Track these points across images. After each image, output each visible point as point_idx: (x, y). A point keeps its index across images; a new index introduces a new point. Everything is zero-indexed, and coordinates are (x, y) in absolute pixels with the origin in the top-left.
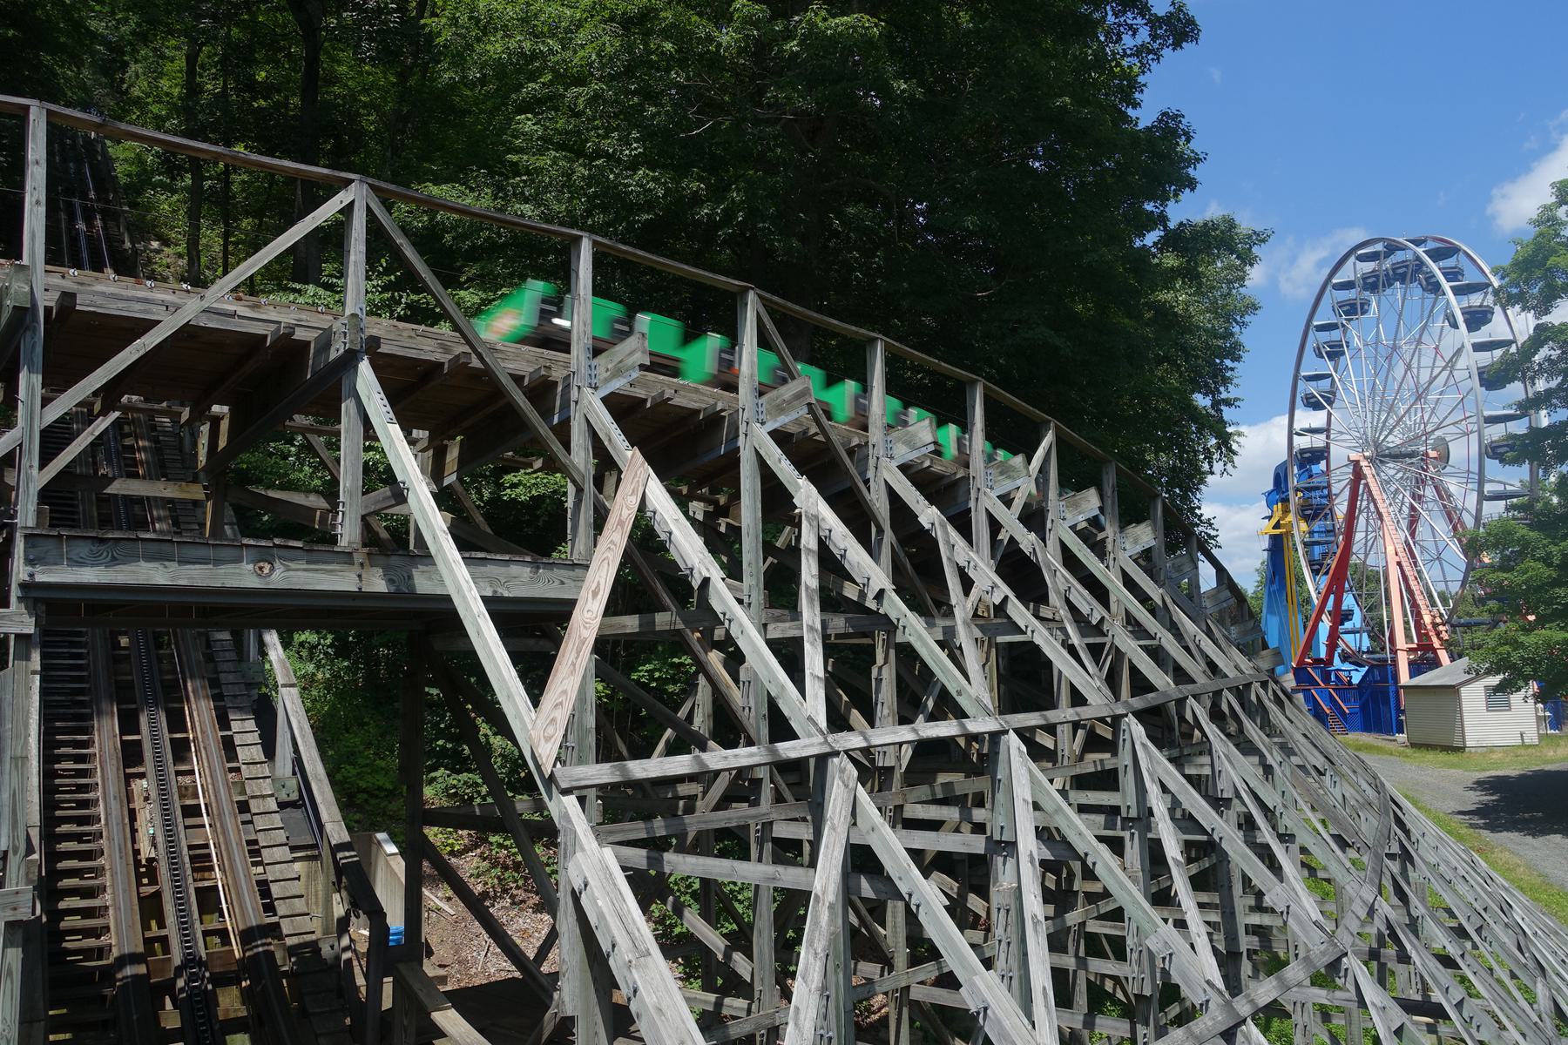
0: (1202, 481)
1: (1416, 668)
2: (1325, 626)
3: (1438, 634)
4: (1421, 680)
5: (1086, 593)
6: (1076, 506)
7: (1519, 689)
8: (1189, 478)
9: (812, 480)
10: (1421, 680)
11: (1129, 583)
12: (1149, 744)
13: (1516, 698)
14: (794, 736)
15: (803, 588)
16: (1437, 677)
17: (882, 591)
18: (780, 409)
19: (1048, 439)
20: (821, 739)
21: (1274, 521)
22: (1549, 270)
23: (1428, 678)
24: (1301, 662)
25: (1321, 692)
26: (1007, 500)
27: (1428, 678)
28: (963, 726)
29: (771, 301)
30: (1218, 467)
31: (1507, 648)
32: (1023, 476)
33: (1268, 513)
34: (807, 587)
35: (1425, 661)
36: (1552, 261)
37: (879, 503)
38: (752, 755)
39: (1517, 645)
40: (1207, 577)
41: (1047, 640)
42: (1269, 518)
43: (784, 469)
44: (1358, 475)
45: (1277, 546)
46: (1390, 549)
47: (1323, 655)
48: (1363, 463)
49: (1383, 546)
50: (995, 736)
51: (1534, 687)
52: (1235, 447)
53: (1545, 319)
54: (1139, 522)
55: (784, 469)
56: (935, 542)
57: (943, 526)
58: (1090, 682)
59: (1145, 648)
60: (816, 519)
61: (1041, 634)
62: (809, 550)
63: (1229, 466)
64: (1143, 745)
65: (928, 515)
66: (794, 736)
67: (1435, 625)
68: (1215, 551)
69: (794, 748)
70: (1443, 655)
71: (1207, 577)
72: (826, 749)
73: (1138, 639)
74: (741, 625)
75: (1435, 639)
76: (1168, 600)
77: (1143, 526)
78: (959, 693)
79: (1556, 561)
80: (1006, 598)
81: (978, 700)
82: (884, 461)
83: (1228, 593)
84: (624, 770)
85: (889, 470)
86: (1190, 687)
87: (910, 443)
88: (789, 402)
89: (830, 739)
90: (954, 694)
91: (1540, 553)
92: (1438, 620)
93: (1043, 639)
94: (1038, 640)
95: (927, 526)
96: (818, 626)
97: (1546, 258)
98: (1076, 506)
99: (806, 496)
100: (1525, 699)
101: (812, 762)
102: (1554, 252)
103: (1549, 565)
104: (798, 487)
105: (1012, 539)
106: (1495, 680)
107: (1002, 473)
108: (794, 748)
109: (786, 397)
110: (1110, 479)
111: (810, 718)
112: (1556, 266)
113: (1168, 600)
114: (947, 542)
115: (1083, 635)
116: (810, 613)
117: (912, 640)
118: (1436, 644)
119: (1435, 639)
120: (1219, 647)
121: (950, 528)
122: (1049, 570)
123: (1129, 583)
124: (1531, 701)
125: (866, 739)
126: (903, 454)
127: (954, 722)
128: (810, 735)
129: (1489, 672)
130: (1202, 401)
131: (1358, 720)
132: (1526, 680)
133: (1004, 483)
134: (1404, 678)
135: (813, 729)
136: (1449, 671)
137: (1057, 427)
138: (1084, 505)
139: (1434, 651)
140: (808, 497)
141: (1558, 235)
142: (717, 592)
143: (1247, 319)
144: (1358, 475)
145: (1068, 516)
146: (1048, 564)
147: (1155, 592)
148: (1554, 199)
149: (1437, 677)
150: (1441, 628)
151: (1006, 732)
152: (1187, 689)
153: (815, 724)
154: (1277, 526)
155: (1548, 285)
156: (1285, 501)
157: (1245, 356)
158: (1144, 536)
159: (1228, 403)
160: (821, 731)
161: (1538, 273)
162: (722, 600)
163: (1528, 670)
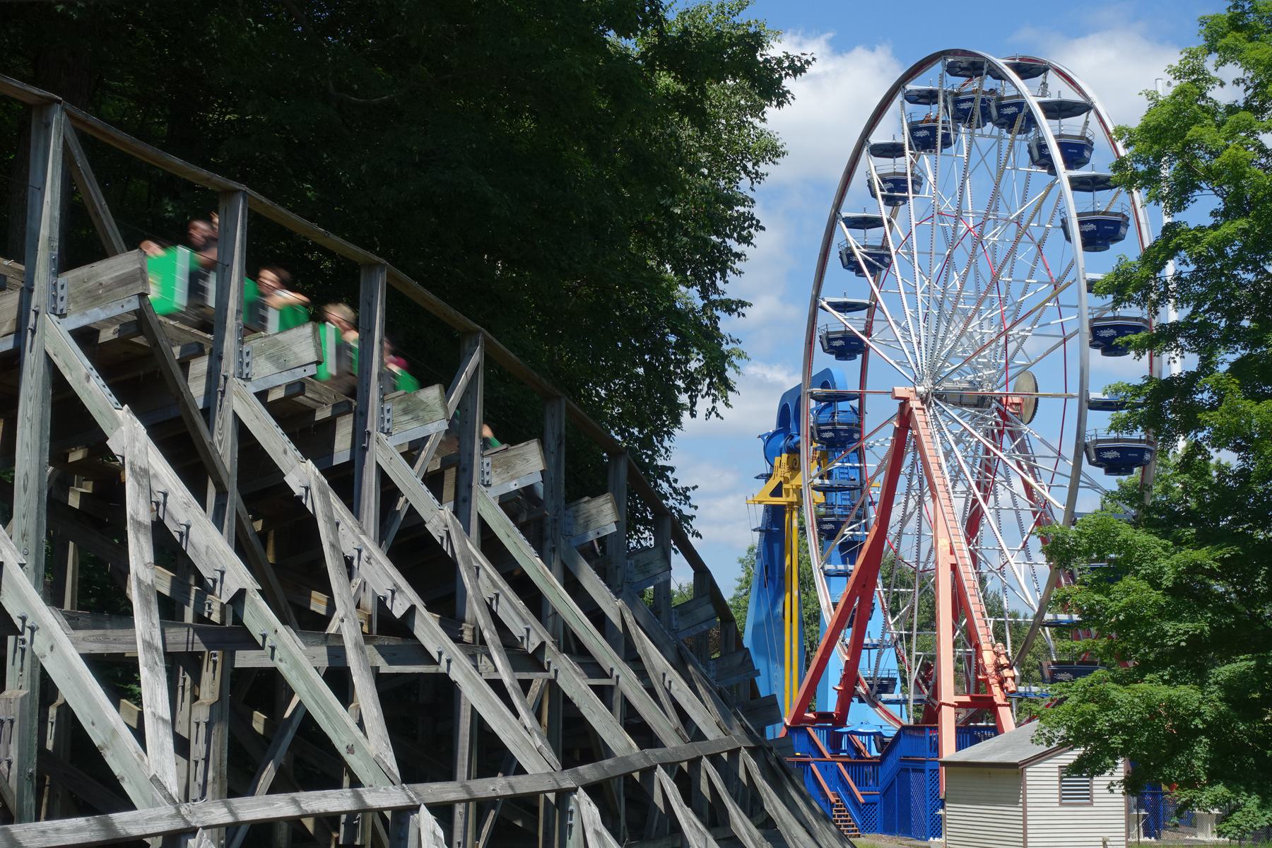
0: (676, 421)
1: (967, 736)
2: (839, 657)
3: (1001, 682)
4: (974, 753)
5: (520, 604)
6: (508, 466)
7: (1102, 772)
8: (659, 412)
9: (139, 412)
10: (974, 753)
11: (491, 545)
12: (606, 833)
13: (1100, 783)
14: (130, 806)
15: (132, 576)
16: (995, 750)
17: (241, 593)
18: (93, 297)
19: (476, 359)
20: (171, 810)
21: (773, 483)
22: (1187, 144)
23: (978, 752)
24: (798, 718)
25: (825, 768)
26: (411, 454)
27: (978, 752)
28: (359, 797)
29: (84, 123)
30: (703, 404)
31: (1093, 707)
32: (431, 413)
33: (764, 468)
34: (140, 582)
35: (979, 720)
36: (1194, 131)
37: (224, 447)
38: (79, 830)
39: (1107, 704)
40: (681, 576)
41: (468, 676)
42: (768, 477)
43: (94, 392)
44: (905, 418)
45: (775, 525)
46: (943, 544)
47: (832, 706)
48: (915, 404)
49: (931, 533)
50: (403, 814)
51: (1120, 770)
52: (730, 373)
53: (1178, 217)
54: (595, 495)
55: (94, 392)
56: (312, 519)
57: (324, 494)
58: (522, 735)
59: (598, 690)
60: (144, 474)
61: (459, 665)
62: (139, 524)
63: (720, 405)
64: (598, 833)
65: (301, 474)
66: (130, 806)
67: (999, 668)
68: (693, 540)
69: (136, 822)
70: (1007, 716)
71: (681, 576)
72: (178, 825)
73: (590, 676)
74: (50, 637)
75: (996, 690)
76: (629, 619)
77: (601, 500)
78: (350, 750)
79: (1167, 582)
80: (413, 608)
81: (377, 761)
82: (234, 384)
83: (709, 609)
84: (109, 826)
85: (242, 398)
86: (658, 751)
87: (279, 360)
88: (109, 288)
89: (183, 810)
90: (342, 751)
91: (1145, 569)
92: (1003, 661)
93: (460, 671)
94: (455, 675)
95: (298, 491)
96: (158, 643)
97: (1188, 127)
98: (508, 466)
99: (128, 436)
100: (1110, 788)
101: (344, 817)
102: (1196, 120)
103: (1155, 585)
104: (117, 424)
105: (412, 511)
106: (1071, 757)
107: (406, 412)
108: (136, 822)
109: (105, 279)
110: (555, 421)
111: (155, 780)
112: (1199, 139)
113: (629, 619)
114: (330, 518)
115: (515, 667)
116: (145, 626)
117: (283, 668)
118: (998, 697)
119: (996, 690)
120: (701, 699)
121: (333, 496)
122: (469, 567)
123: (491, 545)
124: (1119, 790)
125: (231, 812)
126: (267, 374)
127: (347, 791)
128: (154, 804)
129: (1066, 745)
130: (690, 296)
131: (878, 813)
132: (1114, 757)
133: (407, 424)
134: (949, 751)
135: (159, 796)
136: (1012, 739)
137: (487, 343)
138: (520, 467)
139: (993, 707)
140: (134, 439)
141: (1203, 96)
142: (14, 586)
143: (762, 168)
144: (905, 418)
145: (495, 480)
146: (468, 557)
147: (611, 605)
148: (1202, 42)
149: (995, 750)
150: (1006, 673)
151: (416, 809)
152: (654, 754)
153: (162, 787)
154: (777, 492)
155: (1187, 167)
156: (794, 451)
157: (758, 237)
158: (528, 465)
159: (731, 307)
160: (170, 798)
161: (1177, 147)
162: (24, 600)
163: (1117, 741)
